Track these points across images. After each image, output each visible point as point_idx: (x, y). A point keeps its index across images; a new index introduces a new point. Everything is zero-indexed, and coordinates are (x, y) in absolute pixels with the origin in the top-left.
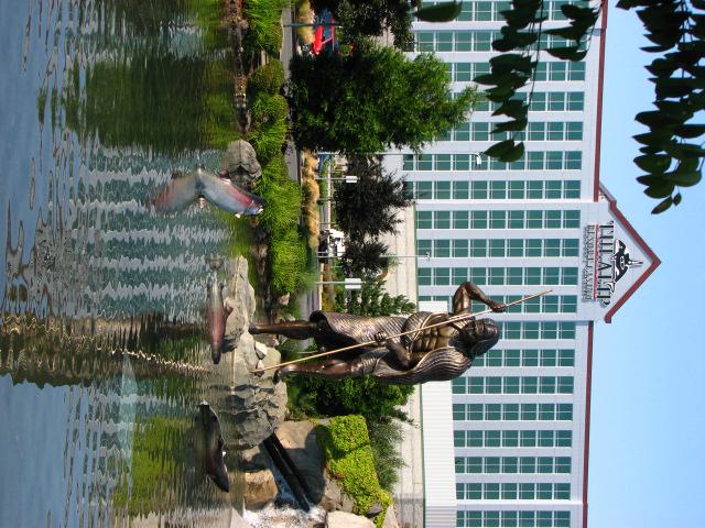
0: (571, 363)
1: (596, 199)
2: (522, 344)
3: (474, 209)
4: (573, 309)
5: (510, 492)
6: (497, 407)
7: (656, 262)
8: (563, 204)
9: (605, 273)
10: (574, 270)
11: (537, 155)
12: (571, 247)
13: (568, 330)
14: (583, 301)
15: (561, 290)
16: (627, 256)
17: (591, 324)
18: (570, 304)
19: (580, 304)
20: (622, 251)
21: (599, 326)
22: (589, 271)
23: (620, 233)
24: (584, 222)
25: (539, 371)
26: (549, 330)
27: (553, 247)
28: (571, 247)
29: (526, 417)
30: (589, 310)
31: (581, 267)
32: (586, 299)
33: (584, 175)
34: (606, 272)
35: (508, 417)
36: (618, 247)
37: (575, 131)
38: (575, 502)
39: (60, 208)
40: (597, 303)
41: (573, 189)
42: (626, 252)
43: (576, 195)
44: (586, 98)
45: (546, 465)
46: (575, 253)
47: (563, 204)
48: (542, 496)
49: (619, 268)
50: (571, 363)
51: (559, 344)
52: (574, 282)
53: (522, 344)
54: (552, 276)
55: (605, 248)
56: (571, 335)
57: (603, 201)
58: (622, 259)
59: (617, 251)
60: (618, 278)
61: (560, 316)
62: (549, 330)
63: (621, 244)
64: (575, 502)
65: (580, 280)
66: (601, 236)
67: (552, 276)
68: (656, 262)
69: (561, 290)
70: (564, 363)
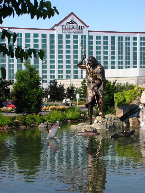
0: (100, 37)
1: (55, 30)
2: (94, 50)
4: (85, 36)
7: (72, 13)
8: (56, 39)
9: (75, 28)
12: (68, 37)
15: (80, 39)
16: (70, 21)
17: (89, 31)
18: (83, 37)
19: (84, 34)
20: (69, 23)
21: (90, 29)
23: (64, 23)
26: (91, 43)
28: (68, 37)
29: (115, 49)
31: (73, 34)
32: (82, 32)
33: (48, 33)
37: (36, 35)
38: (138, 36)
41: (52, 36)
42: (69, 22)
44: (27, 33)
46: (70, 36)
47: (56, 39)
51: (94, 40)
52: (77, 36)
53: (94, 50)
54: (76, 42)
55: (68, 27)
56: (92, 37)
57: (55, 28)
58: (71, 23)
59: (69, 24)
60: (76, 24)
61: (87, 40)
62: (91, 43)
64: (138, 36)
65: (77, 34)
66: (65, 28)
67: (76, 42)
68: (72, 13)
69: (80, 39)
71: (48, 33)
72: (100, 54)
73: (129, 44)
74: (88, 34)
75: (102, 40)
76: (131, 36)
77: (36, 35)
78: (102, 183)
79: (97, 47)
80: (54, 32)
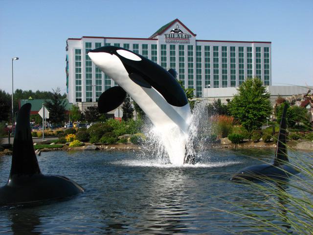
0: (209, 47)
1: (157, 39)
3: (85, 47)
4: (192, 46)
5: (250, 66)
10: (180, 46)
11: (171, 65)
12: (173, 47)
13: (199, 48)
15: (186, 51)
17: (197, 41)
18: (190, 47)
19: (190, 44)
20: (174, 31)
21: (197, 38)
22: (180, 41)
23: (168, 32)
24: (165, 44)
25: (211, 57)
26: (199, 54)
27: (172, 53)
28: (173, 47)
30: (192, 42)
31: (179, 44)
33: (150, 43)
34: (180, 36)
35: (218, 67)
37: (216, 48)
38: (253, 45)
39: (84, 37)
40: (190, 39)
41: (154, 47)
42: (174, 30)
43: (156, 46)
44: (223, 46)
45: (241, 55)
46: (174, 46)
47: (158, 50)
48: (156, 54)
49: (178, 32)
50: (147, 45)
51: (203, 51)
52: (183, 46)
54: (181, 53)
55: (173, 36)
56: (200, 47)
57: (157, 37)
58: (176, 31)
60: (182, 32)
61: (194, 51)
62: (199, 54)
63: (171, 31)
64: (253, 45)
65: (183, 44)
66: (170, 37)
67: (181, 53)
68: (177, 20)
69: (186, 51)
70: (226, 50)
71: (150, 43)
75: (211, 51)
76: (245, 46)
80: (157, 43)
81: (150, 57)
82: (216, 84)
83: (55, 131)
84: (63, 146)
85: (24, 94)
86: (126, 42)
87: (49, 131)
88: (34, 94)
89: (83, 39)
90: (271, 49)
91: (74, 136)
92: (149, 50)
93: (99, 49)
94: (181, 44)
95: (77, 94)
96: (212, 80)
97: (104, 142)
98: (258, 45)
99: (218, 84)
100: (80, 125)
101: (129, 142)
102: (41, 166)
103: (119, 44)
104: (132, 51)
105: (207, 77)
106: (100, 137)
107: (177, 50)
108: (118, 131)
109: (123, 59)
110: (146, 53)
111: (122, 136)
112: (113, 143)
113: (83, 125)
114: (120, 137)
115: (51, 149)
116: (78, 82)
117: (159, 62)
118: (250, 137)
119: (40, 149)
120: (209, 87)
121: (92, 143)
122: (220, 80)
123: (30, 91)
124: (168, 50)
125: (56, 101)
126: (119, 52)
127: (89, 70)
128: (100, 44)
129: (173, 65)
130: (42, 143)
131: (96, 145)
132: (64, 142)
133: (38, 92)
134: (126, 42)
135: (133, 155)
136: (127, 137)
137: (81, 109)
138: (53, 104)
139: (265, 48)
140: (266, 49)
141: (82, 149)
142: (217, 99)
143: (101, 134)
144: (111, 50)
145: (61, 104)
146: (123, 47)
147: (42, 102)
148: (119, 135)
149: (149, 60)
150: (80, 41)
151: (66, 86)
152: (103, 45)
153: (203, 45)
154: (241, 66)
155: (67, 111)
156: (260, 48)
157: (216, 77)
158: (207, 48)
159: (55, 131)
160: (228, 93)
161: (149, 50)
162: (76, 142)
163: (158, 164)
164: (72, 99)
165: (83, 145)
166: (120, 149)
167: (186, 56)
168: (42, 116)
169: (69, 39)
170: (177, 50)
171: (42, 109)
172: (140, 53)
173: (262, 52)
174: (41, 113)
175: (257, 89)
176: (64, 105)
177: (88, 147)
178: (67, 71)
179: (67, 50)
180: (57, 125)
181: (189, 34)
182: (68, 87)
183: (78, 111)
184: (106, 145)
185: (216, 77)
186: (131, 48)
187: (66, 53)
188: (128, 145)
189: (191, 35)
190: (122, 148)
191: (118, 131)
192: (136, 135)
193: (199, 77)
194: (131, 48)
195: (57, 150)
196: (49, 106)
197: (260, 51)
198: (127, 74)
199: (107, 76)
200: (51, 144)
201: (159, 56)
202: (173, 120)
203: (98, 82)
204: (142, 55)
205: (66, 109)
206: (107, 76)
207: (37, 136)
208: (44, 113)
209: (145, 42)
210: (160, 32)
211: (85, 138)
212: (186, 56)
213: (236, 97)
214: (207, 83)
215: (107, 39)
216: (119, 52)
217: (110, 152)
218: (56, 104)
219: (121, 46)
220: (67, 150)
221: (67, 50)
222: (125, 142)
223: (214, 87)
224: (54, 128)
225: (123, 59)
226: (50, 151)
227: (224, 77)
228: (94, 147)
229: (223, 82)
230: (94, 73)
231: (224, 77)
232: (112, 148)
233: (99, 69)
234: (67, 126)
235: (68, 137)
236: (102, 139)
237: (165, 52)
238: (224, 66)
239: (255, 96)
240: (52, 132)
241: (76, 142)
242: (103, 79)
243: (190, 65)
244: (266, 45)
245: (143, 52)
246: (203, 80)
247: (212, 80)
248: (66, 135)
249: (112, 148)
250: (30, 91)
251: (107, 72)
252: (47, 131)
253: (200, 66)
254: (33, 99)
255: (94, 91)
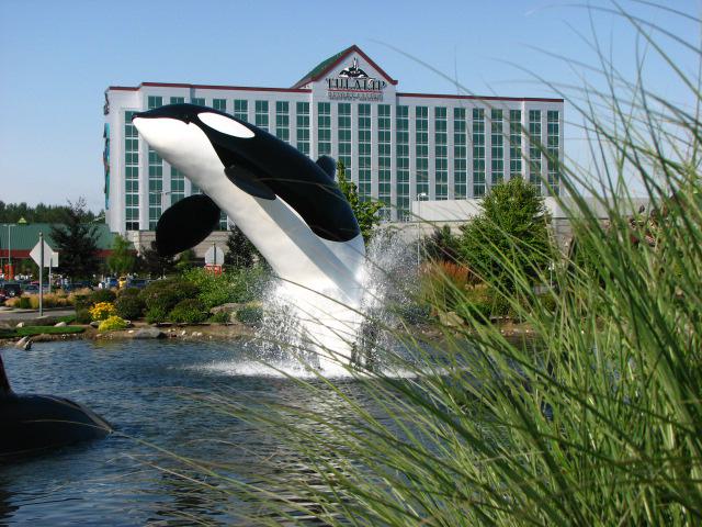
0: (425, 109)
1: (309, 91)
2: (334, 141)
4: (388, 107)
6: (456, 162)
8: (313, 115)
9: (362, 85)
12: (345, 109)
13: (402, 111)
14: (382, 100)
15: (374, 116)
16: (351, 69)
17: (398, 95)
18: (384, 110)
20: (347, 73)
21: (400, 88)
23: (334, 74)
25: (431, 132)
26: (402, 124)
27: (344, 122)
28: (345, 109)
29: (368, 138)
31: (358, 102)
33: (293, 100)
34: (362, 83)
36: (343, 76)
37: (441, 112)
38: (522, 106)
39: (144, 84)
41: (303, 107)
42: (347, 70)
44: (419, 105)
46: (348, 106)
47: (313, 115)
48: (307, 123)
50: (286, 104)
51: (412, 118)
52: (368, 107)
53: (334, 141)
54: (364, 123)
55: (345, 85)
56: (406, 108)
57: (310, 86)
58: (352, 73)
60: (366, 75)
61: (393, 117)
62: (402, 124)
64: (522, 106)
65: (347, 102)
66: (335, 87)
67: (364, 123)
68: (354, 49)
69: (374, 116)
70: (425, 114)
71: (293, 100)
72: (349, 151)
73: (327, 121)
74: (395, 101)
75: (431, 118)
76: (506, 108)
77: (441, 112)
78: (81, 237)
79: (418, 135)
80: (310, 99)
81: (272, 129)
82: (441, 193)
83: (71, 296)
84: (83, 331)
85: (8, 211)
86: (220, 94)
87: (59, 296)
88: (31, 211)
89: (144, 87)
90: (562, 114)
91: (110, 307)
92: (272, 113)
93: (157, 111)
94: (362, 102)
95: (128, 211)
96: (432, 183)
97: (179, 321)
98: (535, 106)
99: (445, 192)
100: (133, 282)
101: (233, 320)
102: (11, 373)
103: (203, 101)
104: (233, 114)
105: (422, 177)
106: (170, 308)
107: (354, 116)
108: (210, 297)
109: (215, 137)
110: (265, 120)
111: (219, 308)
112: (196, 323)
113: (140, 281)
114: (215, 310)
115: (56, 337)
116: (132, 186)
117: (293, 141)
118: (505, 309)
119: (31, 336)
120: (426, 199)
121: (151, 323)
122: (450, 183)
123: (24, 205)
124: (334, 115)
125: (77, 229)
126: (203, 117)
127: (131, 159)
128: (160, 99)
129: (324, 148)
130: (39, 322)
131: (159, 326)
132: (87, 319)
133: (41, 207)
134: (220, 94)
135: (230, 351)
136: (230, 310)
137: (137, 246)
138: (69, 234)
139: (550, 113)
140: (553, 115)
141: (126, 335)
142: (441, 225)
143: (172, 302)
144: (186, 112)
145: (88, 236)
146: (211, 106)
147: (46, 228)
148: (214, 306)
149: (270, 136)
150: (137, 92)
151: (104, 195)
152: (166, 102)
153: (412, 104)
154: (497, 152)
155: (101, 250)
156: (538, 112)
157: (441, 177)
158: (422, 111)
159: (71, 296)
160: (459, 212)
161: (272, 113)
162: (113, 320)
163: (294, 370)
164: (117, 224)
165: (131, 326)
166: (214, 336)
167: (374, 129)
168: (38, 262)
169: (112, 88)
170: (354, 116)
171: (39, 245)
172: (252, 120)
173: (543, 123)
174: (35, 255)
175: (521, 205)
176: (94, 237)
177: (141, 331)
178: (105, 160)
179: (106, 113)
180: (80, 282)
181: (382, 79)
182: (107, 197)
183: (127, 250)
184: (182, 327)
185: (441, 177)
186: (230, 109)
187: (103, 119)
188: (231, 327)
189: (386, 81)
190: (218, 334)
191: (210, 297)
192: (251, 304)
193: (402, 176)
194: (230, 109)
195: (71, 338)
196: (59, 240)
197: (463, 116)
198: (222, 167)
199: (175, 171)
200: (58, 325)
201: (293, 127)
202: (328, 275)
203: (155, 186)
204: (254, 123)
205: (99, 247)
206: (175, 171)
207: (30, 307)
208: (45, 255)
209: (283, 97)
210: (317, 75)
211: (135, 312)
212: (374, 129)
213: (477, 221)
214: (422, 188)
215: (197, 90)
216: (203, 117)
217: (196, 342)
218: (75, 233)
219: (209, 104)
220: (93, 338)
221: (106, 113)
222: (224, 320)
223: (437, 199)
224: (73, 287)
225: (215, 137)
226: (55, 340)
227: (460, 177)
228: (154, 331)
229: (457, 188)
230: (143, 166)
231: (460, 177)
232: (194, 334)
233: (156, 155)
234: (104, 283)
235: (96, 310)
236: (172, 313)
237: (286, 118)
238: (441, 151)
239: (519, 218)
240: (66, 297)
241: (113, 320)
242: (166, 179)
243: (384, 149)
244: (553, 107)
245: (258, 117)
246: (412, 183)
247: (432, 183)
248: (91, 304)
249: (194, 334)
250: (24, 205)
251: (177, 162)
252: (53, 295)
253: (407, 152)
254: (28, 224)
255: (143, 207)
